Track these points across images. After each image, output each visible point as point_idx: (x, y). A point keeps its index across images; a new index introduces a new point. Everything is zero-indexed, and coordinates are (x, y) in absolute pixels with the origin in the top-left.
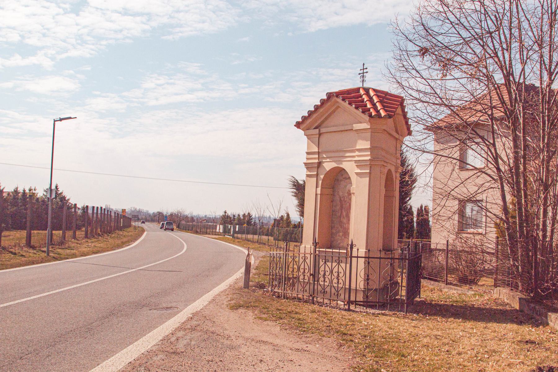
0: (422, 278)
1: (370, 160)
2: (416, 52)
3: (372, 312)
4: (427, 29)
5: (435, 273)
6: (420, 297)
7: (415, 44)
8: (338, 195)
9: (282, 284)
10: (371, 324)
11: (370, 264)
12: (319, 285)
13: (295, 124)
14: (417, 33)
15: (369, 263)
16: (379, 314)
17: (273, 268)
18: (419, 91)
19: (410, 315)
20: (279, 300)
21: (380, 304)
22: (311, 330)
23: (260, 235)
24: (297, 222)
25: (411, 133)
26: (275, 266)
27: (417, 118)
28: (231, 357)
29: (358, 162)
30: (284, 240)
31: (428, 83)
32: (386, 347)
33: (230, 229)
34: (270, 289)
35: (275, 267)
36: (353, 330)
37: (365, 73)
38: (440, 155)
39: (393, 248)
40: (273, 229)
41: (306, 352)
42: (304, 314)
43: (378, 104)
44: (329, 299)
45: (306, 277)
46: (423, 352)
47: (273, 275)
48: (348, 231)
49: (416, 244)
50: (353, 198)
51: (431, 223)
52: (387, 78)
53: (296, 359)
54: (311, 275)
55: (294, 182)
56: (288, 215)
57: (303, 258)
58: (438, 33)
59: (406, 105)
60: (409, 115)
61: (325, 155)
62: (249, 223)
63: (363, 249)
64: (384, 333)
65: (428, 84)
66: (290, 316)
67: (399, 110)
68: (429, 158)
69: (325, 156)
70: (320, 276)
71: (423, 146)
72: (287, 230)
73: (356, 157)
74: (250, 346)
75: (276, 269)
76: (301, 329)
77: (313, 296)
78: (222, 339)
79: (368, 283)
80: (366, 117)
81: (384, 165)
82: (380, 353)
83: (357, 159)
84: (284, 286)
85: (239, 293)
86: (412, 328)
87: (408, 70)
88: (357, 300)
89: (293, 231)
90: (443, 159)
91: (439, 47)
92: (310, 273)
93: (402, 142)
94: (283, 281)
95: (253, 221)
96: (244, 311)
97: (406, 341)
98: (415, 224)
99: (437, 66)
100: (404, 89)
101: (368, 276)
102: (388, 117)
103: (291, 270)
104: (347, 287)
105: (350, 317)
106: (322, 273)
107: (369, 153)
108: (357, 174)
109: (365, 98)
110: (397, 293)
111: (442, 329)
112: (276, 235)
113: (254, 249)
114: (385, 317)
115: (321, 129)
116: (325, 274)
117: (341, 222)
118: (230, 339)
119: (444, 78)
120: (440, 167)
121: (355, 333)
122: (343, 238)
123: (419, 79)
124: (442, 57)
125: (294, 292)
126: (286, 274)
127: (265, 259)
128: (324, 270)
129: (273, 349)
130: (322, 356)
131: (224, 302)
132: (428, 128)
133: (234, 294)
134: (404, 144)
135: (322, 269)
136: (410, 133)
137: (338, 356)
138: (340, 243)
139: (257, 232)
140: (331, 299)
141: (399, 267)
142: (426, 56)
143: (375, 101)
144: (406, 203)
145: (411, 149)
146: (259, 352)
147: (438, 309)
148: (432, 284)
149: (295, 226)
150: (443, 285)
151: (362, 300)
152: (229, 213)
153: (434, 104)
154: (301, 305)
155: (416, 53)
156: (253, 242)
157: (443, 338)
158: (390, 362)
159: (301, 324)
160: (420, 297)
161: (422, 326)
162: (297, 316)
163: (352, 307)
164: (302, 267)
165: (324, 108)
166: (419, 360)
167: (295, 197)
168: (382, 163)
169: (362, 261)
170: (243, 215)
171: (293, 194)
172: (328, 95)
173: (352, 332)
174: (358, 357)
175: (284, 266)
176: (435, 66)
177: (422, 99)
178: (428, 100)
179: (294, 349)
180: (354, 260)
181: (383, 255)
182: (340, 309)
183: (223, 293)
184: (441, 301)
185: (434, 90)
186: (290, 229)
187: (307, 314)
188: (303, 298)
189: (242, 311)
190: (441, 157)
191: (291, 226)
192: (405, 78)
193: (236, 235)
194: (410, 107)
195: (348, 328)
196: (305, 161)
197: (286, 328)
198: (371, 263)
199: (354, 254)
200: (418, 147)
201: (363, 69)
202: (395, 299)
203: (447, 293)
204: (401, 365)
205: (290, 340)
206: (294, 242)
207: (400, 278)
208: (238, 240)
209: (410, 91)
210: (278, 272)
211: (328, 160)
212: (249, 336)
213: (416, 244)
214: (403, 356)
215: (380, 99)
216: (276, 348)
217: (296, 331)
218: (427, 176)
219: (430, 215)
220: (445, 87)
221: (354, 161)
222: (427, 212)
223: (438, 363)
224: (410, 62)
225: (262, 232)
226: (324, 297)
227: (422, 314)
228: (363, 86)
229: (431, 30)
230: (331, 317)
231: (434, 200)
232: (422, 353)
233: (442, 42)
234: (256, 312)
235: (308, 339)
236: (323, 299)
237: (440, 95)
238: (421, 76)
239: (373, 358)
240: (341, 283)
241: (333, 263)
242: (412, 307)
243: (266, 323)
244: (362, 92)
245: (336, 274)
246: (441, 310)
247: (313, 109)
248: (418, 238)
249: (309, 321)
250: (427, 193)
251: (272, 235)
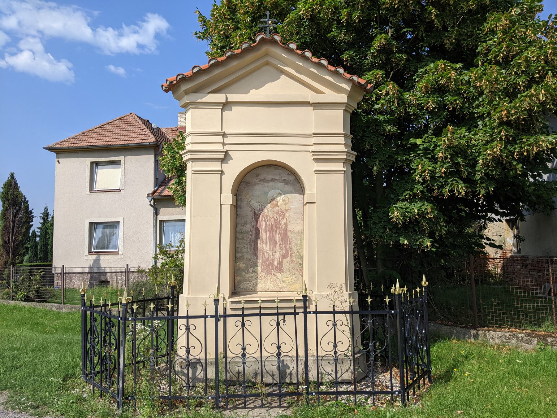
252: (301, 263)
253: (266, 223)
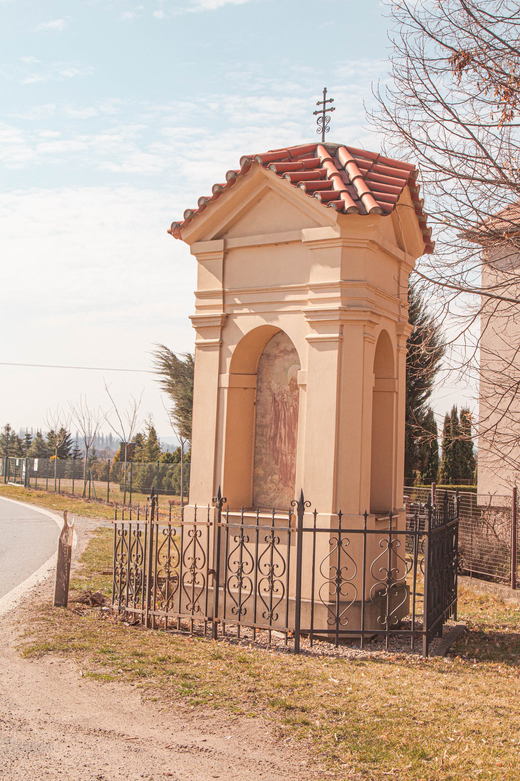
0: (460, 575)
1: (340, 309)
2: (444, 61)
3: (349, 655)
4: (470, 7)
5: (487, 563)
6: (455, 619)
7: (441, 43)
8: (270, 389)
9: (144, 595)
10: (349, 683)
11: (343, 545)
12: (227, 593)
13: (169, 228)
14: (446, 18)
15: (340, 543)
16: (365, 659)
17: (122, 558)
18: (448, 152)
19: (436, 661)
20: (138, 631)
21: (366, 636)
22: (212, 702)
23: (90, 480)
24: (173, 447)
25: (433, 249)
26: (126, 552)
27: (445, 213)
28: (30, 773)
29: (313, 314)
30: (144, 492)
31: (471, 134)
32: (384, 736)
33: (19, 467)
34: (116, 607)
35: (127, 556)
36: (307, 697)
37: (329, 110)
38: (498, 297)
39: (394, 509)
40: (118, 468)
41: (202, 754)
42: (195, 663)
43: (357, 183)
44: (252, 628)
45: (199, 578)
46: (469, 747)
47: (122, 573)
48: (293, 471)
49: (446, 497)
50: (304, 396)
51: (475, 449)
52: (379, 122)
53: (181, 771)
54: (209, 572)
55: (166, 359)
56: (153, 432)
57: (192, 534)
58: (494, 17)
59: (421, 183)
60: (429, 207)
61: (239, 299)
62: (63, 453)
63: (327, 512)
64: (378, 705)
65: (469, 136)
66: (164, 669)
67: (406, 197)
68: (473, 304)
69: (238, 301)
70: (230, 574)
71: (458, 278)
72: (150, 467)
73: (309, 303)
74: (74, 743)
75: (130, 560)
76: (189, 698)
77: (215, 620)
78: (8, 729)
79: (339, 590)
80: (332, 213)
81: (371, 322)
82: (371, 752)
83: (310, 307)
84: (149, 599)
85: (44, 619)
86: (441, 690)
87: (426, 103)
88: (315, 628)
89: (165, 469)
90: (504, 305)
91: (496, 49)
92: (208, 569)
93: (412, 268)
94: (147, 587)
95: (73, 447)
96: (58, 660)
97: (428, 722)
98: (440, 452)
99: (491, 95)
100: (417, 148)
101: (339, 573)
102: (380, 211)
103: (164, 561)
104: (293, 597)
105: (300, 669)
106: (235, 568)
107: (338, 294)
108: (311, 341)
109: (329, 168)
110: (404, 611)
111: (509, 693)
112: (127, 479)
113: (80, 513)
114: (379, 665)
115: (229, 240)
116: (241, 569)
117: (276, 451)
118: (25, 728)
119: (507, 122)
120: (498, 323)
121: (313, 705)
122: (281, 486)
123: (450, 125)
124: (502, 73)
125: (171, 613)
126: (153, 569)
127: (102, 537)
128: (239, 560)
129: (127, 749)
130: (238, 761)
131: (10, 640)
132: (469, 235)
133: (33, 620)
134: (416, 271)
135: (235, 557)
136: (429, 249)
137: (276, 759)
138: (274, 499)
139: (82, 473)
140: (256, 625)
141: (407, 550)
142: (467, 70)
143: (352, 176)
144: (419, 403)
145: (431, 283)
146: (94, 756)
147: (498, 645)
148: (483, 588)
149: (169, 459)
150: (507, 589)
151: (326, 628)
152: (17, 430)
153: (484, 181)
154: (187, 642)
155: (443, 64)
156: (73, 496)
157: (513, 713)
158: (394, 771)
159: (189, 687)
160: (455, 619)
161: (464, 686)
162: (180, 669)
163: (305, 644)
164: (189, 553)
165: (235, 192)
166: (461, 767)
167: (170, 392)
168: (368, 317)
169: (324, 539)
170: (49, 434)
171: (166, 387)
172: (243, 163)
173: (305, 703)
174: (322, 763)
175: (148, 551)
176: (486, 94)
177: (456, 170)
178: (470, 172)
179: (174, 746)
180: (307, 537)
181: (371, 524)
182: (277, 649)
183: (7, 620)
184: (504, 627)
185: (484, 150)
186: (158, 464)
187: (202, 662)
188: (193, 625)
189: (52, 661)
190: (499, 300)
191: (161, 459)
192: (419, 123)
193: (32, 481)
194: (429, 189)
195: (296, 694)
196: (193, 312)
197: (154, 697)
198: (345, 543)
199: (308, 523)
200: (448, 278)
201: (325, 102)
202: (402, 624)
203: (516, 607)
204: (420, 778)
205: (166, 725)
206: (168, 494)
207: (411, 575)
208: (38, 492)
209: (430, 152)
210: (134, 567)
211: (246, 310)
212: (70, 718)
213: (446, 497)
214: (423, 756)
215: (361, 172)
216: (133, 746)
217: (177, 704)
218: (468, 343)
219: (473, 433)
220: (509, 143)
221: (305, 312)
222: (467, 423)
223: (503, 773)
224: (430, 86)
225: (94, 472)
226: (240, 623)
227: (463, 658)
228: (323, 141)
229: (478, 10)
230: (256, 668)
231: (483, 398)
232: (467, 749)
233: (503, 38)
234: (85, 663)
235: (207, 722)
236: (239, 626)
237: (497, 162)
238: (455, 117)
239: (356, 763)
240: (277, 590)
241: (259, 545)
242: (439, 641)
243: (108, 686)
244: (321, 154)
245: (266, 570)
246: (504, 648)
247: (210, 194)
248: (448, 483)
249: (208, 680)
250: (468, 382)
251: (116, 480)
253: (285, 413)
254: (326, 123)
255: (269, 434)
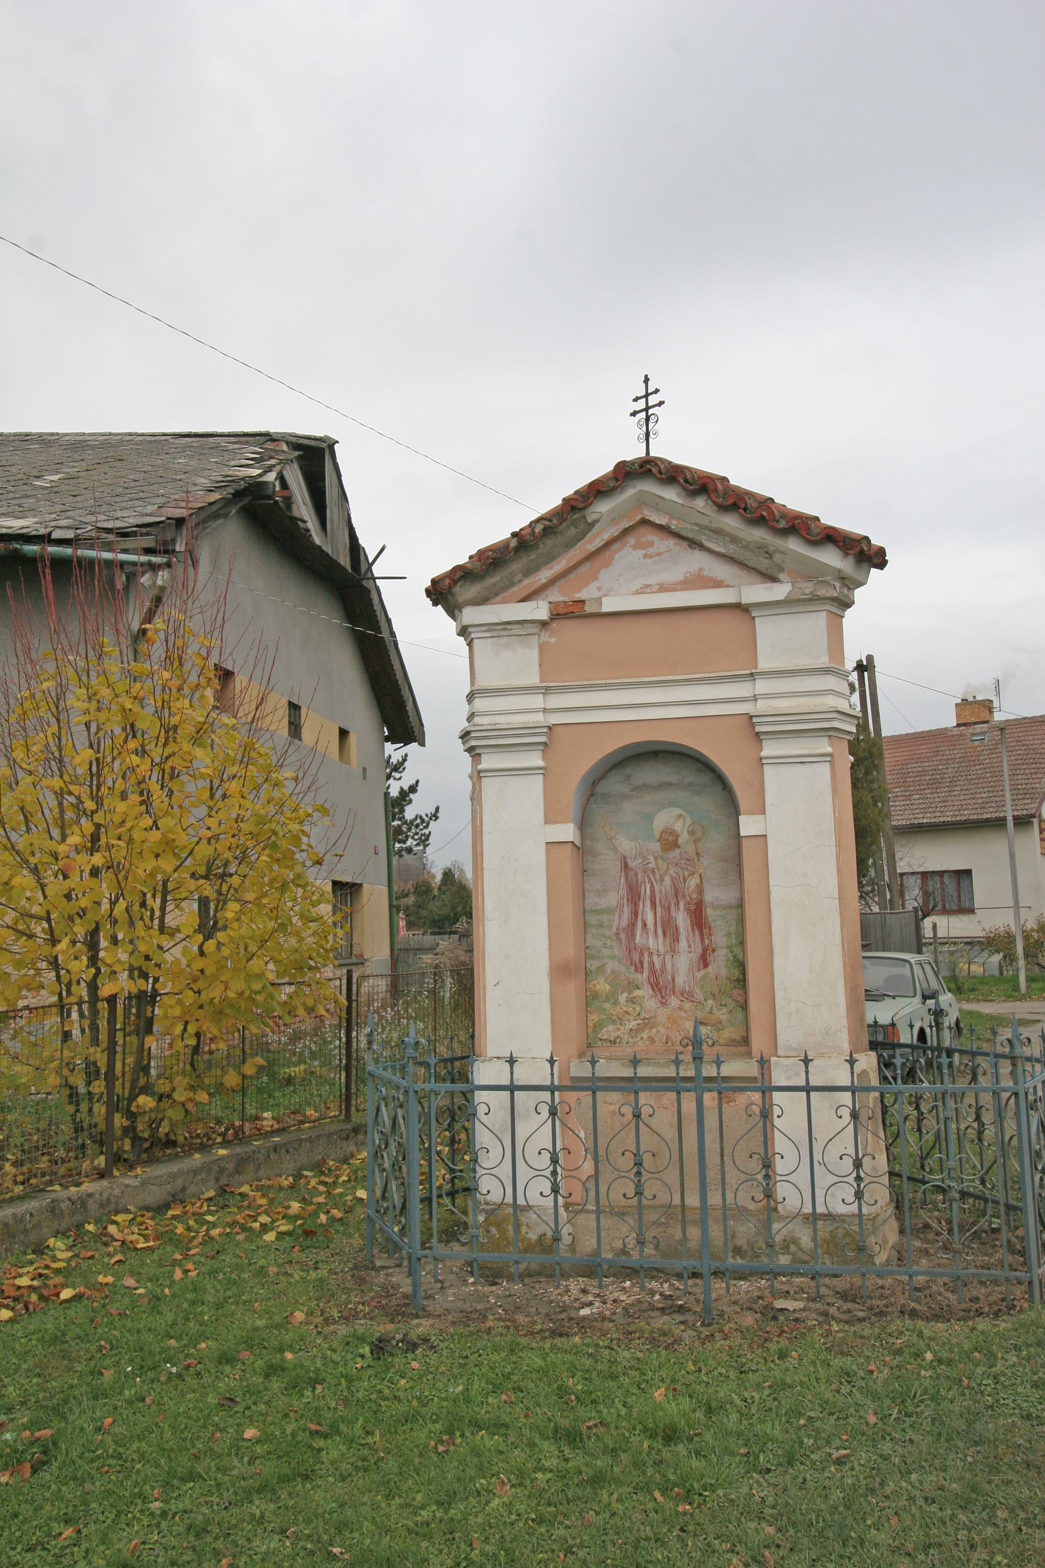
201: (647, 395)
252: (741, 977)
253: (652, 886)
254: (651, 425)
255: (616, 923)
